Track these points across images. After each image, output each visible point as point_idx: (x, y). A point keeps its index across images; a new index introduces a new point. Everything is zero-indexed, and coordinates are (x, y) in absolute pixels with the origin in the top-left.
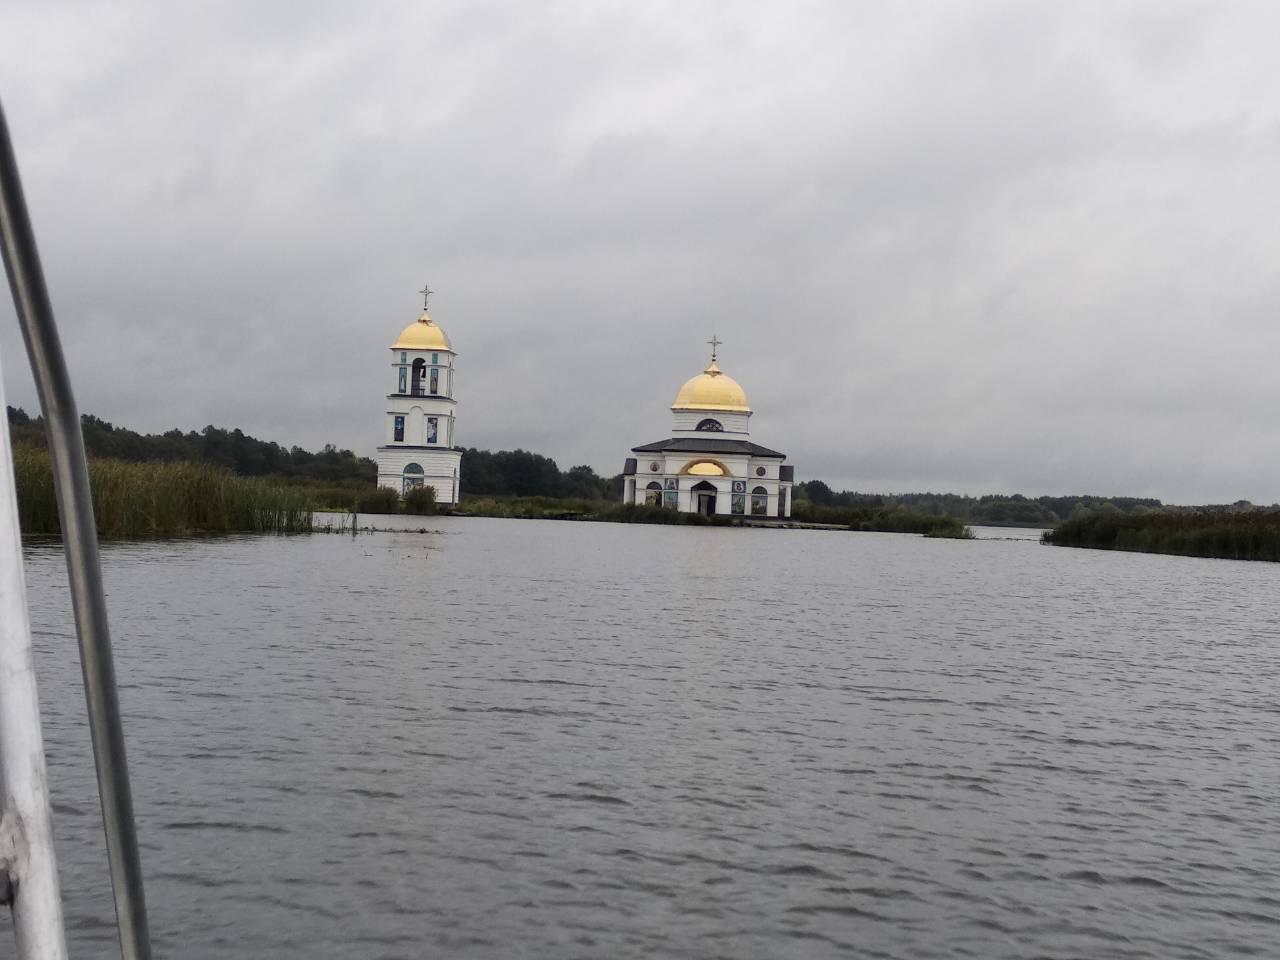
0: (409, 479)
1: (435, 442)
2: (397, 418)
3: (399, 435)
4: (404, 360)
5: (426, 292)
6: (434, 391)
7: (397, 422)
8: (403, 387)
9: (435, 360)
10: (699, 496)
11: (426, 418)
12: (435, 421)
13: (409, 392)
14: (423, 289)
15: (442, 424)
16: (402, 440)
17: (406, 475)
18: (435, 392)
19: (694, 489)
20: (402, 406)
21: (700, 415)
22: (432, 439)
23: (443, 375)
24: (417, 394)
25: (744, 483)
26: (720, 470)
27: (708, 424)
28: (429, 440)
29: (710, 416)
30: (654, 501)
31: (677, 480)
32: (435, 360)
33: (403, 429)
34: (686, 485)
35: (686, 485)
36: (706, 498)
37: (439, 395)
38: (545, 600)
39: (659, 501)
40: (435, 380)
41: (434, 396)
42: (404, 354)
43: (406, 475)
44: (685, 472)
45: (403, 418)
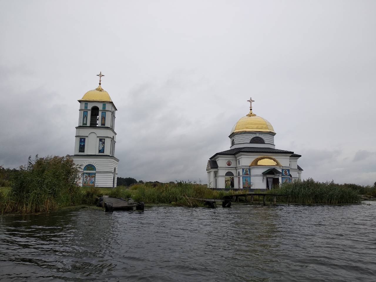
0: (87, 173)
1: (103, 152)
2: (81, 139)
3: (82, 148)
4: (86, 107)
5: (101, 75)
6: (103, 124)
7: (81, 141)
8: (85, 122)
9: (104, 107)
10: (267, 178)
11: (98, 139)
12: (103, 141)
13: (88, 124)
14: (102, 74)
15: (108, 142)
16: (84, 151)
17: (85, 171)
18: (104, 125)
19: (264, 174)
20: (84, 132)
21: (251, 134)
22: (102, 151)
23: (108, 115)
24: (93, 125)
25: (289, 170)
26: (275, 162)
27: (257, 140)
28: (100, 151)
29: (258, 135)
30: (230, 183)
31: (250, 169)
32: (104, 107)
33: (84, 145)
34: (257, 172)
35: (257, 172)
36: (271, 180)
37: (106, 126)
38: (196, 244)
39: (232, 184)
40: (104, 118)
41: (103, 126)
42: (86, 104)
43: (85, 171)
44: (255, 164)
45: (84, 139)
